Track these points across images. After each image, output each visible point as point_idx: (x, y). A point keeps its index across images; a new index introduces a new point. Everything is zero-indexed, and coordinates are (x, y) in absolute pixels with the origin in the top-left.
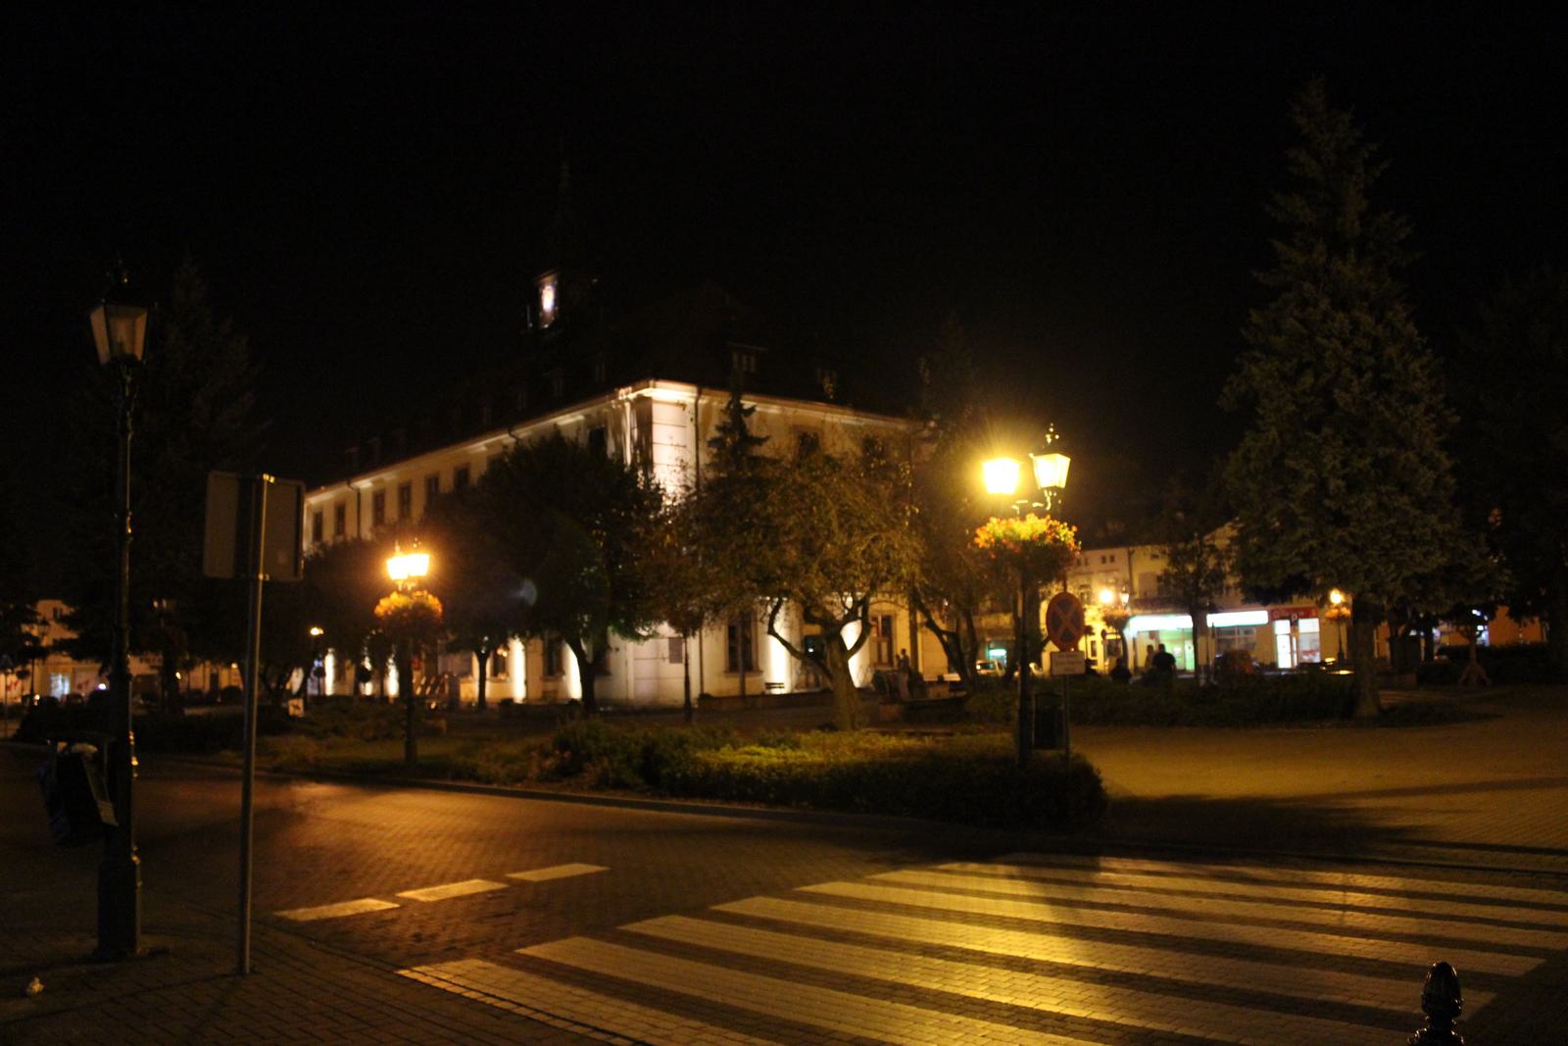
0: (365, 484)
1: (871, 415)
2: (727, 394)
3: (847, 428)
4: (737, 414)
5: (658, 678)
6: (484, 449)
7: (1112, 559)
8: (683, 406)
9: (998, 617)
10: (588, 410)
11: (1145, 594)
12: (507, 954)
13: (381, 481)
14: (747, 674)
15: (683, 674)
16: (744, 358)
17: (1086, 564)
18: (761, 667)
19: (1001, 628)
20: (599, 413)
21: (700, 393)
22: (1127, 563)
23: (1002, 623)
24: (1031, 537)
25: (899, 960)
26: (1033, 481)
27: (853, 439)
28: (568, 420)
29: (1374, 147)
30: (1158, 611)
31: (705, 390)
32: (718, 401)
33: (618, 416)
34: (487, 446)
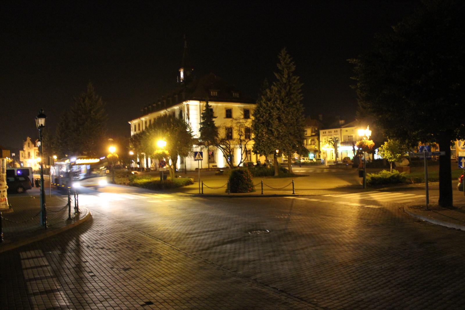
0: (143, 119)
1: (244, 104)
2: (205, 102)
3: (239, 107)
4: (207, 106)
5: (191, 165)
6: (163, 113)
7: (337, 131)
8: (197, 105)
9: (311, 146)
10: (179, 106)
11: (345, 141)
12: (176, 264)
13: (146, 118)
14: (210, 163)
15: (198, 163)
16: (236, 94)
17: (331, 132)
18: (216, 161)
19: (312, 149)
20: (181, 107)
21: (200, 102)
22: (340, 132)
23: (312, 148)
24: (152, 139)
25: (307, 284)
26: (243, 118)
27: (241, 110)
28: (176, 108)
29: (293, 63)
30: (347, 145)
31: (201, 102)
32: (204, 104)
33: (184, 107)
34: (164, 112)
